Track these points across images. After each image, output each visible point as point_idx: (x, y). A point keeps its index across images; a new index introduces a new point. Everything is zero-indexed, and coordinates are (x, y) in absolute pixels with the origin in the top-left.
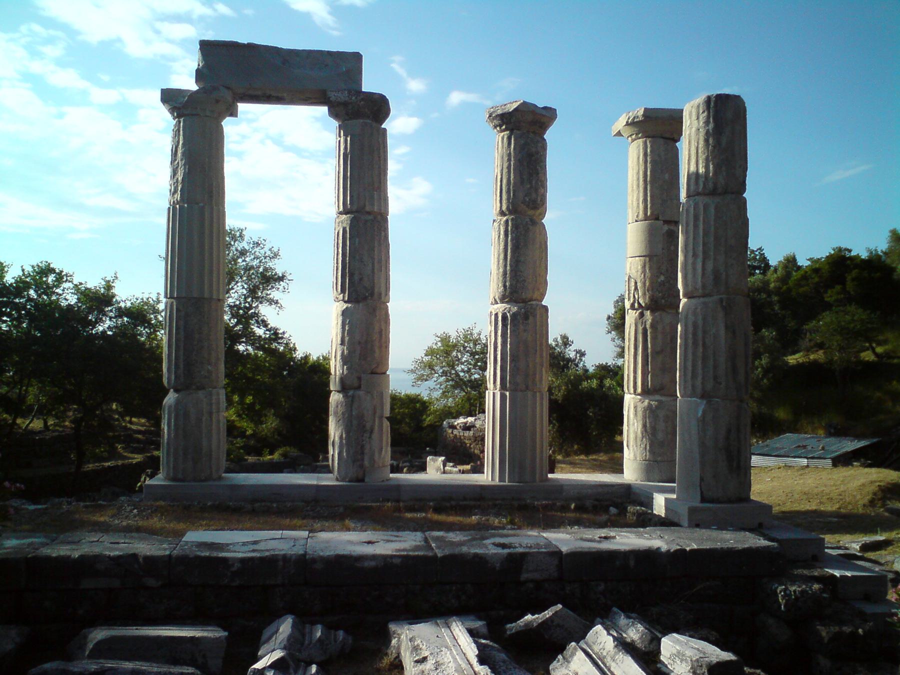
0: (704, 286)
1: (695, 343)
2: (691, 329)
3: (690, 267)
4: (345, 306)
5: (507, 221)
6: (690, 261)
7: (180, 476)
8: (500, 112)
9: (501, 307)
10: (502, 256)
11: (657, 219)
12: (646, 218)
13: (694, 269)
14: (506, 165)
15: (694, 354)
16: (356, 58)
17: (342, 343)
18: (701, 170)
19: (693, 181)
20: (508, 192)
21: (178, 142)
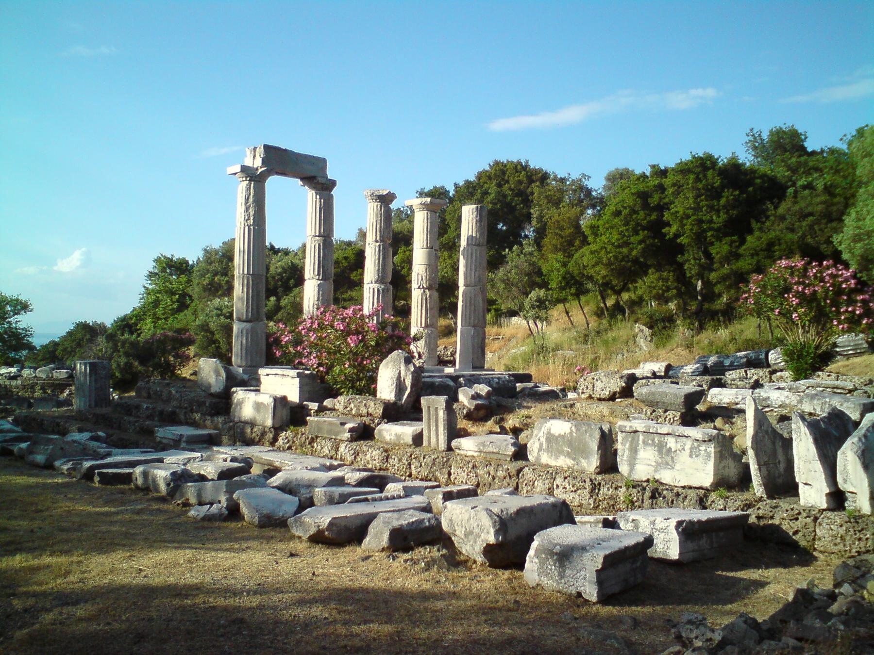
0: (473, 282)
1: (470, 305)
2: (469, 299)
3: (468, 274)
4: (319, 282)
5: (380, 245)
6: (469, 271)
7: (254, 364)
8: (377, 193)
9: (376, 286)
10: (377, 261)
11: (432, 248)
12: (427, 248)
13: (471, 275)
14: (379, 219)
15: (470, 309)
16: (324, 161)
17: (318, 300)
18: (474, 235)
19: (470, 239)
20: (380, 231)
21: (250, 194)
